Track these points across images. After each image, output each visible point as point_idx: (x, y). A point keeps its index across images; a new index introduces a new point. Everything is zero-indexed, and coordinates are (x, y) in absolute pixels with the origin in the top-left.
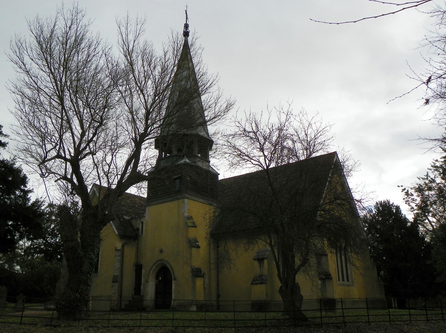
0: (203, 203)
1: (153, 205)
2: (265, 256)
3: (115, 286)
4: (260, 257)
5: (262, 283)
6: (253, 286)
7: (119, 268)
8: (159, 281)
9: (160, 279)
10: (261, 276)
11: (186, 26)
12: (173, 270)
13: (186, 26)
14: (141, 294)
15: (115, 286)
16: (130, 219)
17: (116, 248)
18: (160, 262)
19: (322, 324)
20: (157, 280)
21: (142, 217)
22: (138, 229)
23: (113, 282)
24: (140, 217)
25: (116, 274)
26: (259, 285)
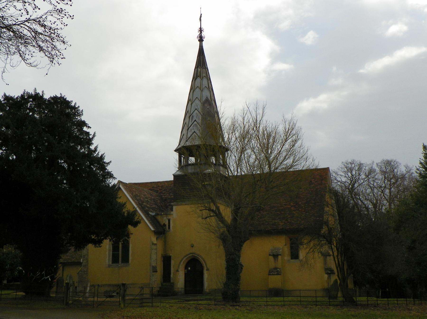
1: (182, 205)
2: (280, 253)
3: (155, 275)
4: (275, 254)
5: (277, 274)
6: (270, 276)
8: (188, 270)
9: (189, 268)
10: (276, 268)
11: (201, 30)
13: (201, 30)
14: (171, 281)
17: (152, 242)
19: (368, 305)
20: (186, 270)
21: (169, 214)
22: (165, 225)
26: (275, 276)
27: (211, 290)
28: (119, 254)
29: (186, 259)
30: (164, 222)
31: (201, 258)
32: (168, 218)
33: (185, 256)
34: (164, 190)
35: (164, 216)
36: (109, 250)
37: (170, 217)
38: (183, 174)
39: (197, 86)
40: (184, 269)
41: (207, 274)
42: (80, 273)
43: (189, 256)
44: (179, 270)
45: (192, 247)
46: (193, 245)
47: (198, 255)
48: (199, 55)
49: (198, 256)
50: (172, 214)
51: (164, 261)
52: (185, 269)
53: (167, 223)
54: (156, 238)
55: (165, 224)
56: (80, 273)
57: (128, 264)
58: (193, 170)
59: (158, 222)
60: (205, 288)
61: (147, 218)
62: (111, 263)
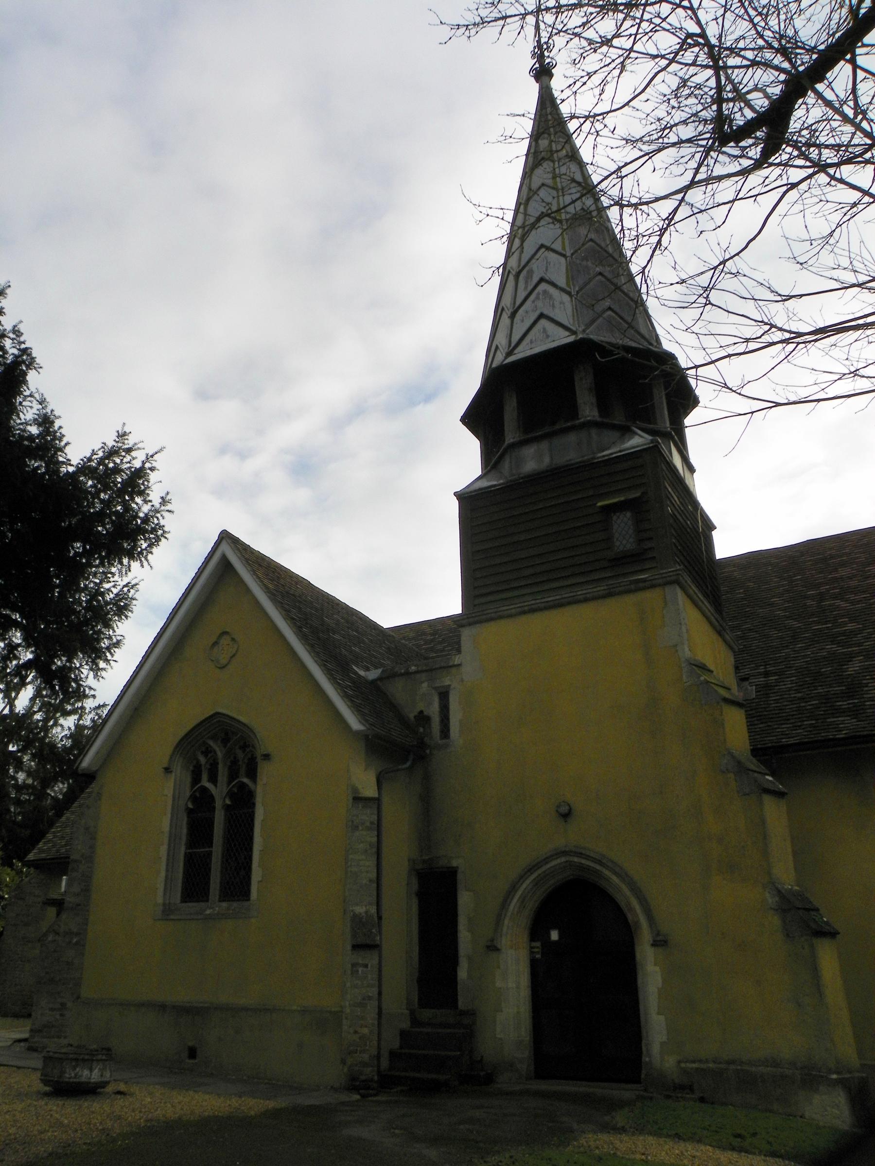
0: (707, 618)
1: (501, 617)
7: (370, 881)
9: (554, 935)
12: (643, 901)
15: (366, 966)
16: (380, 679)
17: (355, 790)
18: (563, 859)
20: (538, 944)
22: (423, 719)
23: (356, 947)
24: (431, 670)
25: (360, 910)
27: (694, 1065)
28: (210, 854)
29: (537, 883)
30: (421, 706)
31: (615, 873)
32: (437, 685)
33: (531, 870)
34: (440, 643)
35: (418, 676)
36: (173, 838)
37: (447, 682)
38: (501, 481)
39: (540, 184)
40: (523, 938)
41: (657, 969)
42: (50, 938)
43: (548, 866)
44: (504, 942)
45: (566, 815)
46: (569, 805)
47: (600, 863)
48: (539, 108)
49: (598, 867)
50: (459, 665)
51: (423, 896)
52: (533, 936)
53: (434, 710)
54: (373, 780)
55: (425, 713)
56: (50, 938)
57: (246, 904)
58: (547, 460)
59: (394, 707)
60: (656, 1049)
61: (332, 675)
62: (179, 901)
